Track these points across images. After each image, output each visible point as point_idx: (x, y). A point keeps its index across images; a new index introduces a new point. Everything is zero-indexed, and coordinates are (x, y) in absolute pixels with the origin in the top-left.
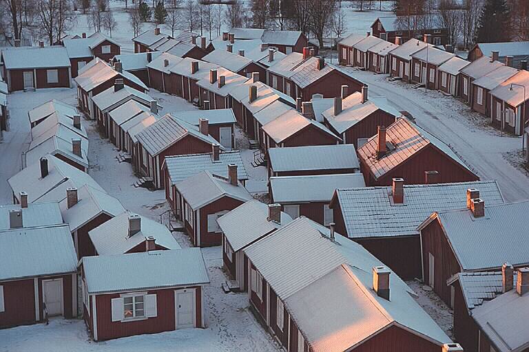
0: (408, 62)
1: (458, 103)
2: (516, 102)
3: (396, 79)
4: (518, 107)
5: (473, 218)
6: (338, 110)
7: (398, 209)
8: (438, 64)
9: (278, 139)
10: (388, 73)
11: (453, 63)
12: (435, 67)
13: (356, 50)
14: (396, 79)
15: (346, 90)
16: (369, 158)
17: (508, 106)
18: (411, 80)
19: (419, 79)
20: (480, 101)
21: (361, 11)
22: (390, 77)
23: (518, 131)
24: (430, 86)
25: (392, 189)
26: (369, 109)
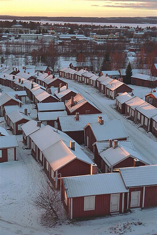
2: (113, 89)
7: (77, 122)
12: (88, 78)
18: (81, 82)
19: (84, 82)
23: (114, 98)
24: (87, 84)
26: (69, 91)
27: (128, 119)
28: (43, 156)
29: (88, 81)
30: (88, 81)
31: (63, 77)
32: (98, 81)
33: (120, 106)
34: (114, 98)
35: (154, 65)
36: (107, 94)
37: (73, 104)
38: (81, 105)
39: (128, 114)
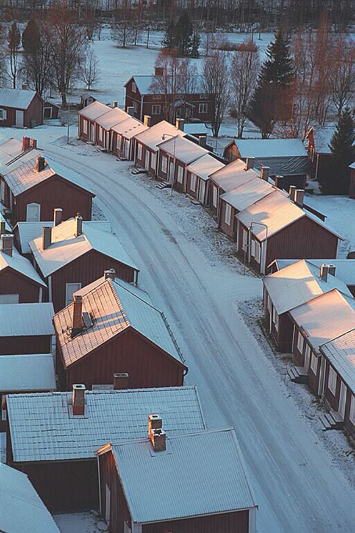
0: (154, 153)
1: (206, 216)
2: (262, 236)
3: (141, 172)
4: (263, 241)
5: (152, 452)
6: (48, 244)
7: (76, 422)
8: (187, 162)
9: (18, 182)
10: (132, 160)
11: (206, 166)
12: (183, 165)
13: (98, 125)
14: (141, 172)
15: (60, 214)
16: (63, 332)
17: (254, 237)
18: (156, 176)
19: (165, 176)
20: (228, 221)
21: (124, 47)
22: (135, 166)
23: (263, 269)
24: (177, 187)
25: (71, 395)
26: (83, 247)
27: (297, 380)
28: (193, 135)
29: (180, 174)
30: (180, 174)
31: (93, 138)
32: (217, 187)
33: (275, 319)
34: (263, 269)
35: (306, 285)
36: (241, 245)
37: (81, 326)
38: (106, 338)
39: (299, 361)
